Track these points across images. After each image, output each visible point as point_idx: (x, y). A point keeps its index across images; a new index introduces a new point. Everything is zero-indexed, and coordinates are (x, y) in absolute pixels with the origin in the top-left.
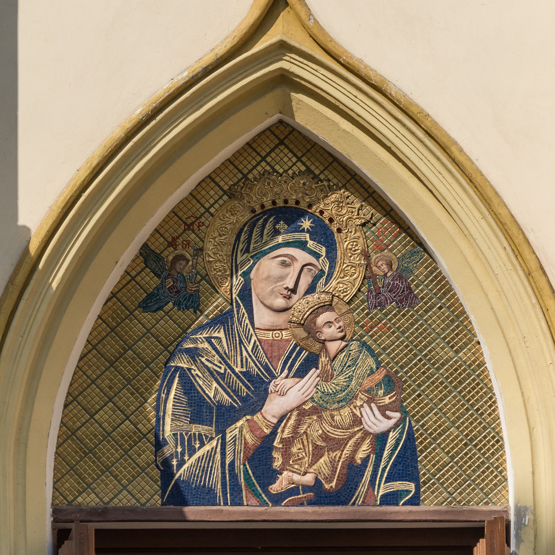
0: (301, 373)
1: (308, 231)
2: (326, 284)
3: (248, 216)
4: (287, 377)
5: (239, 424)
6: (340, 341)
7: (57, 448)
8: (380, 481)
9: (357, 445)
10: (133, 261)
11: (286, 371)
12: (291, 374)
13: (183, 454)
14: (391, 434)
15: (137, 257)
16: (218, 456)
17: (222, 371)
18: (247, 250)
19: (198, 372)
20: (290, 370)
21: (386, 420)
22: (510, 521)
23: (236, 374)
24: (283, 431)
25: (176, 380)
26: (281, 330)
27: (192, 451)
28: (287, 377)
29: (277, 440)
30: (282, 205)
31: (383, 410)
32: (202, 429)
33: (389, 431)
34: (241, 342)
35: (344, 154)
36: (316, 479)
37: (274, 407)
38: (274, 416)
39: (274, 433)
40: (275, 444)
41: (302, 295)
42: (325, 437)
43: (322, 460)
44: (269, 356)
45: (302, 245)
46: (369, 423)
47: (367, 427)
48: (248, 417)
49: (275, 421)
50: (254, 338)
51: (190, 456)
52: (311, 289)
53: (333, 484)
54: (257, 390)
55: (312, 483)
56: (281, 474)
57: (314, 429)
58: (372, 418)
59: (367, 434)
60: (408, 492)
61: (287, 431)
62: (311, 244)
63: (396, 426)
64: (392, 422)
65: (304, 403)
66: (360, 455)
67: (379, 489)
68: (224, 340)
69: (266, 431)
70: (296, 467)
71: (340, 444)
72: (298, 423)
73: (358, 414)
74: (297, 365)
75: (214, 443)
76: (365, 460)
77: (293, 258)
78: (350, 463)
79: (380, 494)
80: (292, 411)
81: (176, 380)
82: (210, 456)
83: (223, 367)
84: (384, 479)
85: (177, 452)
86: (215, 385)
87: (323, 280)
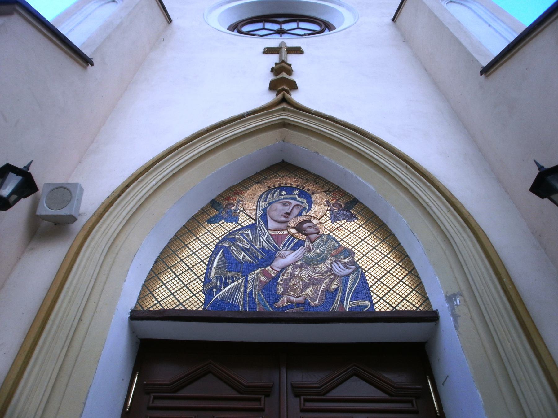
0: (294, 249)
1: (297, 194)
2: (308, 212)
3: (267, 189)
4: (286, 250)
5: (256, 272)
6: (316, 235)
7: (145, 282)
8: (347, 300)
9: (331, 282)
10: (207, 206)
11: (286, 248)
12: (289, 249)
13: (220, 286)
14: (351, 277)
15: (208, 204)
16: (242, 289)
17: (248, 247)
18: (266, 201)
19: (234, 248)
20: (287, 248)
21: (347, 270)
22: (228, 9)
23: (256, 249)
24: (283, 275)
25: (221, 251)
26: (283, 230)
27: (226, 285)
28: (286, 250)
29: (280, 279)
30: (289, 185)
31: (345, 265)
32: (234, 274)
33: (349, 275)
34: (260, 236)
35: (197, 131)
36: (305, 299)
37: (279, 263)
38: (278, 268)
39: (278, 276)
40: (279, 281)
41: (295, 215)
42: (310, 278)
43: (308, 289)
44: (276, 241)
45: (295, 199)
46: (337, 271)
47: (336, 273)
48: (263, 268)
49: (279, 270)
50: (267, 233)
51: (225, 287)
52: (300, 214)
53: (317, 302)
54: (268, 257)
55: (304, 301)
56: (282, 297)
57: (305, 274)
58: (339, 268)
59: (335, 276)
60: (367, 306)
61: (286, 275)
62: (298, 199)
63: (353, 272)
64: (351, 271)
65: (297, 262)
66: (334, 287)
67: (347, 303)
68: (250, 235)
69: (273, 275)
70: (292, 293)
71: (321, 281)
72: (293, 271)
73: (330, 267)
74: (291, 246)
75: (240, 281)
76: (336, 290)
77: (290, 203)
78: (327, 291)
79: (348, 307)
80: (289, 266)
81: (221, 251)
82: (237, 288)
83: (249, 246)
84: (349, 300)
85: (217, 285)
86: (243, 253)
87: (306, 211)
